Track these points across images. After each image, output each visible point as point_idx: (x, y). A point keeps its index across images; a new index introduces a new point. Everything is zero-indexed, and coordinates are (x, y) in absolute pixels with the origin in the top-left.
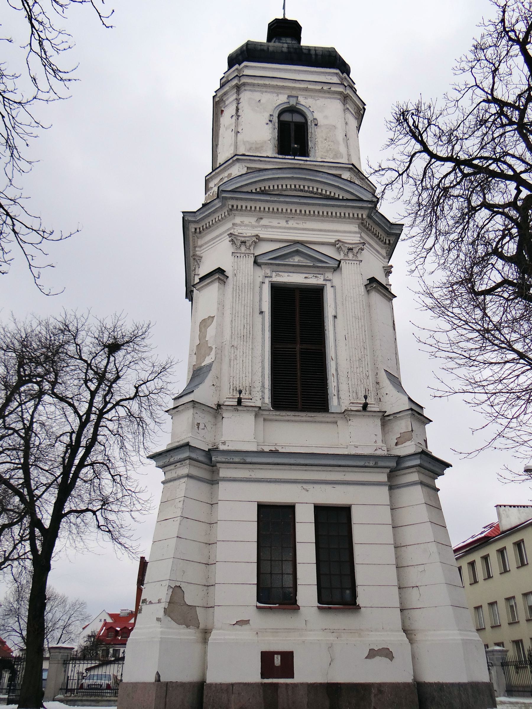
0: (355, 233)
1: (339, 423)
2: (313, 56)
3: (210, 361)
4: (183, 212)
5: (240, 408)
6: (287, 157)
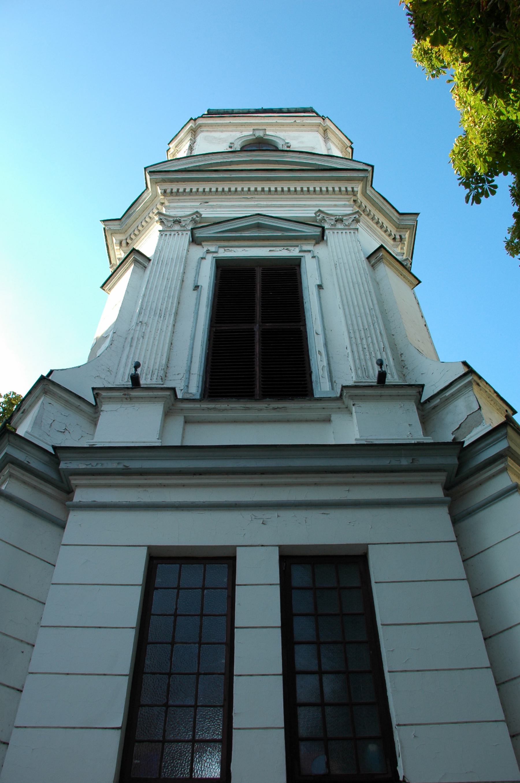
1: (334, 417)
4: (104, 221)
5: (134, 393)
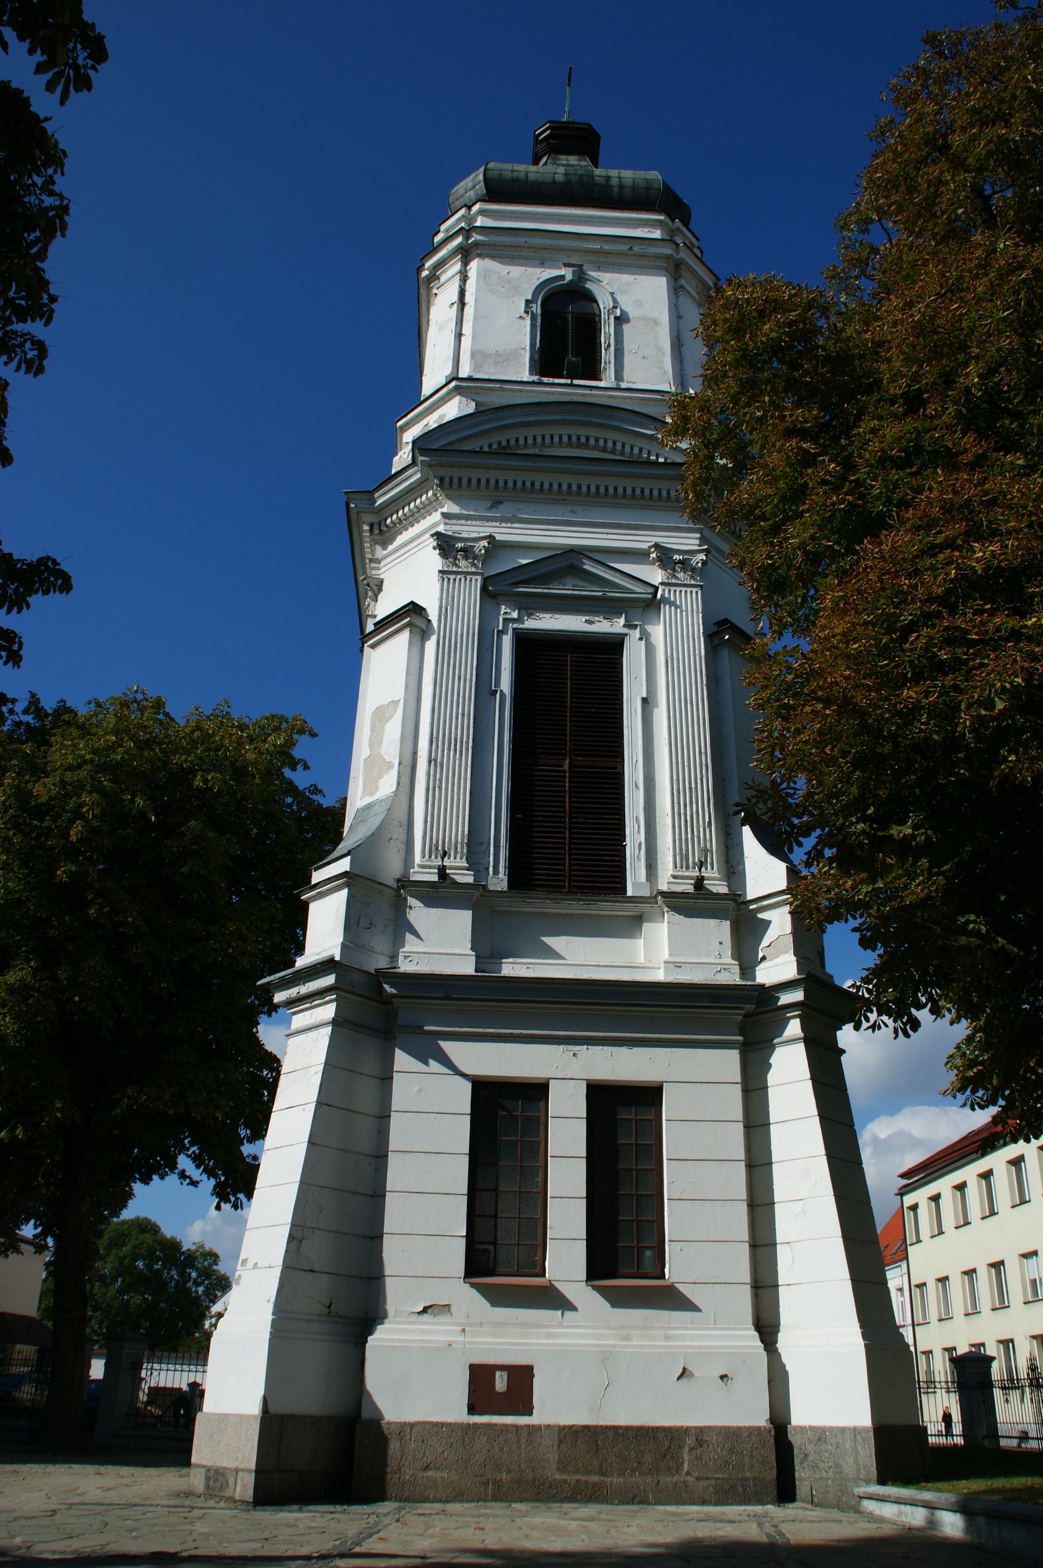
2: (616, 189)
6: (557, 381)
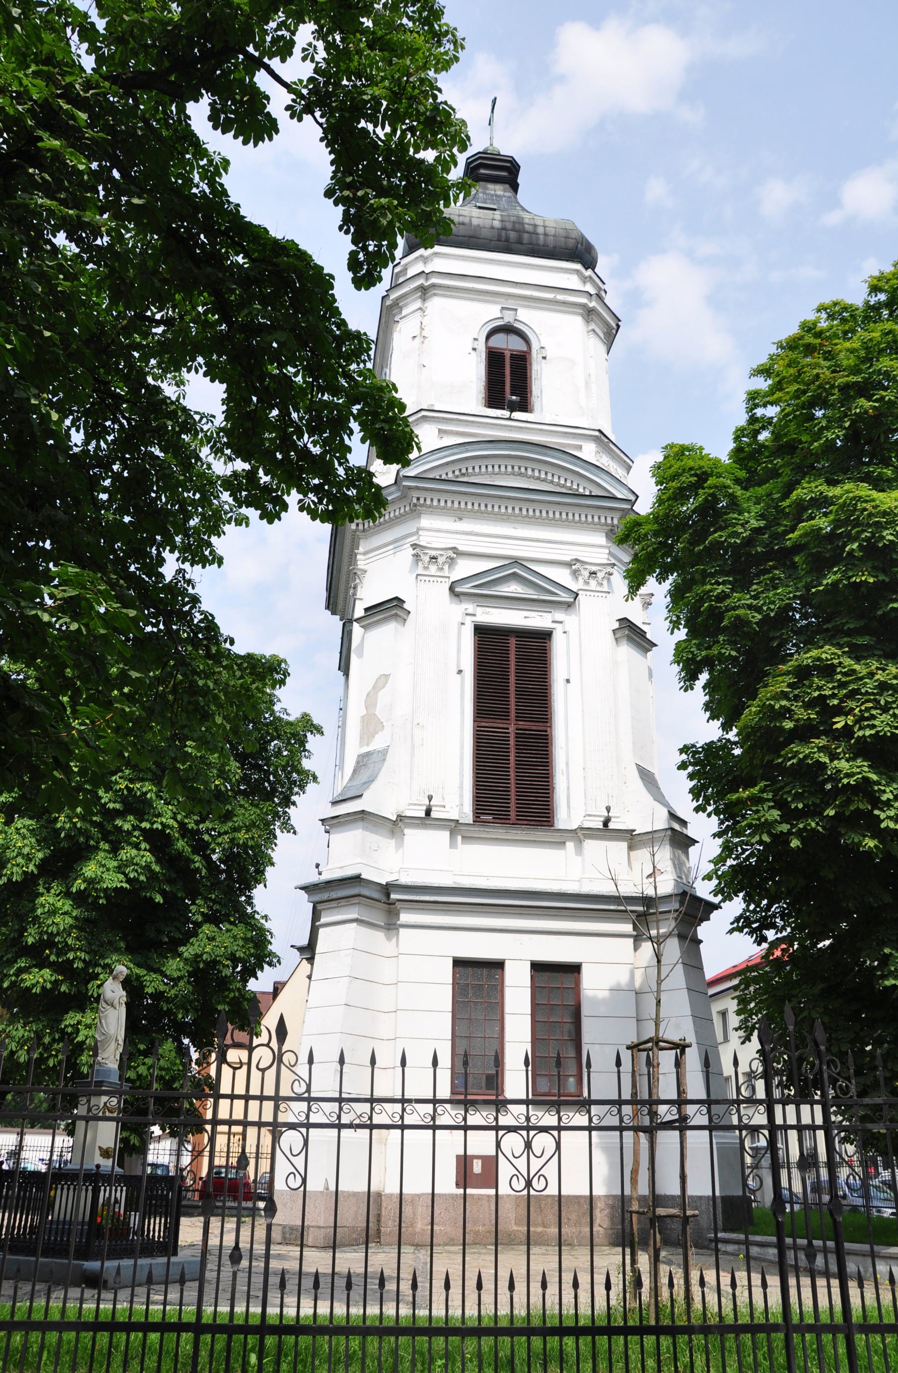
0: (601, 546)
2: (542, 237)
3: (384, 745)
